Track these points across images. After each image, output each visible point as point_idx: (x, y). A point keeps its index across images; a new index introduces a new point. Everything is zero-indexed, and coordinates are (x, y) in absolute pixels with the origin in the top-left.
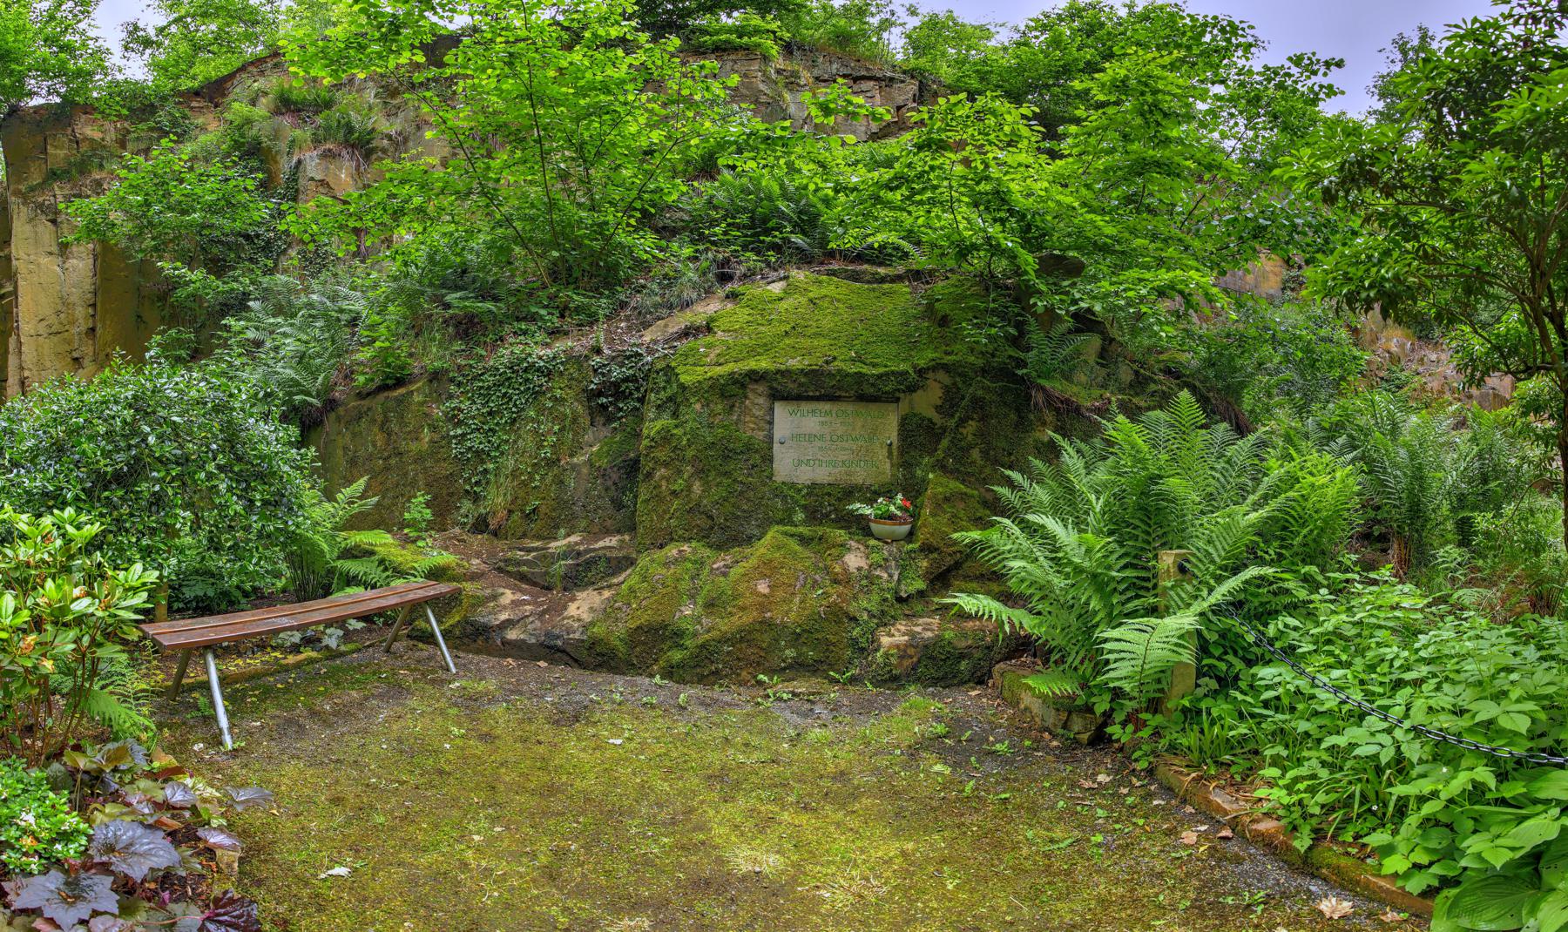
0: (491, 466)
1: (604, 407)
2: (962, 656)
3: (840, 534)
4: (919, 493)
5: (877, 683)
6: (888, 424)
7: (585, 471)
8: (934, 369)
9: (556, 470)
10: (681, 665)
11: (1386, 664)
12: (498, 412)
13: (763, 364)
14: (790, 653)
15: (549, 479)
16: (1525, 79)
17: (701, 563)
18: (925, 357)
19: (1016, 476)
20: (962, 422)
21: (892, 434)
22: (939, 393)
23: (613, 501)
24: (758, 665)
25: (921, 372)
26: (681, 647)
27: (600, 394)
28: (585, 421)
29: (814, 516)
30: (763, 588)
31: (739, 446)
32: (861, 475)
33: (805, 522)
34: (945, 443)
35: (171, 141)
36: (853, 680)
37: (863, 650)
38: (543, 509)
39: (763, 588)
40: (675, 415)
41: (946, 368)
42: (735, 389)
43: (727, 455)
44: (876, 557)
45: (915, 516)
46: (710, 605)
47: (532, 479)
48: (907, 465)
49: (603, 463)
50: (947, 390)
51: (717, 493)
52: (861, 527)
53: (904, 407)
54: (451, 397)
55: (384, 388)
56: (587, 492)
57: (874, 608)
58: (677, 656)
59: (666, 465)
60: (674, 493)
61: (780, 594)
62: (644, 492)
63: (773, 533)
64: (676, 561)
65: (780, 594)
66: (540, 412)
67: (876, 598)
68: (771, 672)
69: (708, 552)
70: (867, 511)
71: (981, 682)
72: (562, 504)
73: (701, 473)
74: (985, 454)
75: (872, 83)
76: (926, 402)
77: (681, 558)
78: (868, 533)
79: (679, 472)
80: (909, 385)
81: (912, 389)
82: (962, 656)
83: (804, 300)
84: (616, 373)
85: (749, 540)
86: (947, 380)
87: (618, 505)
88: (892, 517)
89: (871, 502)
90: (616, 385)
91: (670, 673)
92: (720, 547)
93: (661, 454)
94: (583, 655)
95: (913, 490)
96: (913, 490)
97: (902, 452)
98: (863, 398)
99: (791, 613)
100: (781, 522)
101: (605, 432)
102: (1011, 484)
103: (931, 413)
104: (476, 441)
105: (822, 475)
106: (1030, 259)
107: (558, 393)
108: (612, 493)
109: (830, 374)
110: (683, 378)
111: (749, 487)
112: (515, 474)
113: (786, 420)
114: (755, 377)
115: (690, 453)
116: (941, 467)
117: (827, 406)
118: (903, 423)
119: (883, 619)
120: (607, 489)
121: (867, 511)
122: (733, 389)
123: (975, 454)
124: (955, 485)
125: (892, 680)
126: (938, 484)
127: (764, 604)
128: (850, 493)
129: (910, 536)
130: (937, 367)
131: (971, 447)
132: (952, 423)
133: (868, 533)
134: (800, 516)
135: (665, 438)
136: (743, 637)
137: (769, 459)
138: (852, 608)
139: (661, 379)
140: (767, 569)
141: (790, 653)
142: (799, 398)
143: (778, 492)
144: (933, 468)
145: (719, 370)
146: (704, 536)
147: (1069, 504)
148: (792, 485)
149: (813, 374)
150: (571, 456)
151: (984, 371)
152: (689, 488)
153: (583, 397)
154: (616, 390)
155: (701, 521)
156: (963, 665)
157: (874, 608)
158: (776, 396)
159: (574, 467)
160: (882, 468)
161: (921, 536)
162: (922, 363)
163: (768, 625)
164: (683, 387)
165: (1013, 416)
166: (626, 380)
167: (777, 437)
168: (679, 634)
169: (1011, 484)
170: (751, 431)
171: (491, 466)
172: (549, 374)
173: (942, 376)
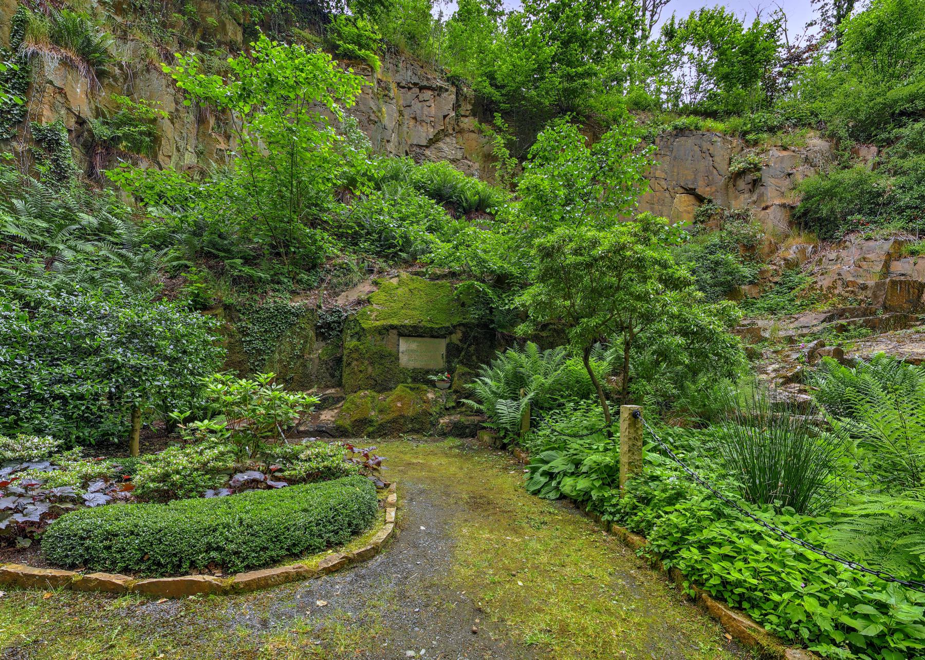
0: (266, 357)
1: (323, 333)
2: (467, 427)
3: (425, 387)
4: (453, 372)
5: (439, 435)
6: (441, 346)
7: (317, 361)
8: (459, 325)
9: (301, 360)
10: (373, 432)
11: (69, 243)
12: (270, 331)
13: (395, 322)
14: (410, 426)
15: (298, 364)
17: (373, 397)
18: (456, 320)
19: (484, 366)
20: (469, 345)
21: (443, 350)
22: (461, 335)
23: (330, 374)
24: (399, 431)
25: (454, 327)
26: (371, 426)
27: (321, 327)
28: (314, 339)
29: (415, 380)
30: (399, 405)
31: (386, 354)
32: (432, 365)
33: (412, 382)
34: (463, 353)
36: (431, 435)
37: (433, 425)
38: (296, 378)
39: (399, 405)
40: (359, 340)
41: (463, 325)
42: (384, 331)
43: (382, 357)
44: (438, 394)
45: (452, 380)
46: (381, 411)
47: (289, 364)
48: (449, 362)
49: (325, 358)
50: (464, 333)
51: (378, 371)
52: (432, 384)
53: (448, 340)
54: (240, 320)
56: (318, 370)
57: (438, 411)
58: (371, 429)
59: (357, 360)
60: (361, 371)
61: (405, 407)
62: (347, 371)
63: (400, 386)
64: (364, 397)
65: (405, 407)
66: (294, 333)
67: (438, 408)
68: (404, 433)
69: (375, 394)
70: (434, 378)
71: (473, 437)
72: (306, 376)
73: (372, 363)
74: (478, 358)
75: (430, 93)
76: (456, 338)
77: (365, 396)
78: (435, 386)
79: (362, 363)
80: (449, 332)
81: (451, 333)
82: (467, 427)
83: (407, 289)
84: (330, 319)
85: (391, 389)
86: (464, 330)
87: (333, 376)
88: (443, 380)
89: (436, 375)
90: (329, 324)
91: (369, 435)
92: (379, 392)
93: (355, 356)
94: (334, 432)
95: (451, 371)
96: (451, 371)
97: (447, 358)
98: (432, 337)
99: (410, 413)
100: (402, 382)
101: (323, 344)
102: (482, 369)
103: (458, 342)
104: (258, 344)
105: (418, 364)
107: (303, 326)
108: (330, 371)
109: (421, 328)
110: (364, 326)
111: (391, 369)
112: (280, 361)
114: (392, 327)
115: (367, 356)
116: (461, 362)
117: (419, 339)
118: (448, 345)
119: (441, 415)
120: (327, 369)
121: (434, 378)
122: (384, 331)
123: (474, 358)
124: (467, 369)
125: (444, 435)
126: (460, 369)
127: (400, 409)
128: (428, 372)
129: (450, 388)
130: (460, 325)
131: (473, 355)
132: (465, 346)
133: (435, 386)
134: (410, 380)
135: (357, 349)
136: (394, 421)
137: (398, 359)
138: (431, 411)
139: (352, 324)
140: (400, 398)
141: (410, 426)
142: (409, 336)
143: (401, 372)
144: (458, 363)
145: (378, 323)
146: (373, 388)
148: (407, 369)
149: (415, 327)
150: (310, 354)
151: (478, 326)
152: (367, 369)
153: (314, 328)
154: (328, 326)
155: (372, 382)
156: (467, 430)
157: (438, 411)
158: (401, 335)
159: (311, 360)
160: (441, 363)
161: (454, 387)
162: (455, 323)
163: (403, 416)
164: (363, 329)
165: (489, 343)
166: (334, 322)
167: (401, 350)
168: (371, 421)
169: (482, 369)
170: (390, 348)
171: (266, 357)
172: (297, 316)
173: (461, 328)
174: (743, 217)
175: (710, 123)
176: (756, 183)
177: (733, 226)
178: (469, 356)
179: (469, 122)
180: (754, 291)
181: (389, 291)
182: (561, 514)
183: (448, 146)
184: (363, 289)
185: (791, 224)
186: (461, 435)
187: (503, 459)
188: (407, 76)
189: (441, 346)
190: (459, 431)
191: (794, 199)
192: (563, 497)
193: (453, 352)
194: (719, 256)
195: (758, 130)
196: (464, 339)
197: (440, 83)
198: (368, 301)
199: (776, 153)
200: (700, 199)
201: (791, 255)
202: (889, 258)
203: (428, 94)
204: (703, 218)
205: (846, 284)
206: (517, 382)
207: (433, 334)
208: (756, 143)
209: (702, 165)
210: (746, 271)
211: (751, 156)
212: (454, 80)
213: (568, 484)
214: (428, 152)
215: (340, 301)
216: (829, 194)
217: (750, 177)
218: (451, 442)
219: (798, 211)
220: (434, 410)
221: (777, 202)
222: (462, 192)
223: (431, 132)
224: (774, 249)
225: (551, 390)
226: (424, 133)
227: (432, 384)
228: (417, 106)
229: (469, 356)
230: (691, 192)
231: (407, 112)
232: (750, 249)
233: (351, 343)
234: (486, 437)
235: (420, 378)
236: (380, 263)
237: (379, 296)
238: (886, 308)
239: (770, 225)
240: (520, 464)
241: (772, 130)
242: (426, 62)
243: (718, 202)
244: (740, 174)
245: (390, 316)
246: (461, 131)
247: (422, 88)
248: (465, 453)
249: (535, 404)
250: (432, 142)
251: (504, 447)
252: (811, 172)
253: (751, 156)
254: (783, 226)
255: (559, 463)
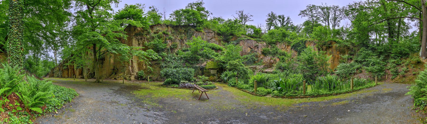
6: (216, 70)
13: (210, 68)
16: (331, 8)
18: (218, 67)
29: (213, 75)
32: (215, 73)
35: (377, 102)
52: (215, 76)
55: (106, 96)
76: (218, 70)
80: (217, 69)
99: (213, 79)
105: (213, 73)
106: (166, 54)
113: (211, 71)
119: (217, 79)
122: (209, 69)
125: (217, 82)
126: (219, 74)
135: (205, 71)
147: (224, 75)
154: (201, 68)
158: (211, 69)
160: (216, 73)
170: (210, 71)
174: (256, 52)
175: (252, 39)
176: (258, 48)
177: (255, 53)
178: (220, 72)
179: (216, 36)
180: (257, 62)
181: (208, 63)
182: (231, 87)
183: (213, 40)
184: (205, 63)
185: (262, 53)
186: (219, 82)
187: (225, 84)
188: (207, 31)
189: (216, 70)
190: (219, 81)
191: (262, 50)
192: (232, 86)
193: (217, 71)
194: (253, 57)
195: (258, 41)
196: (219, 70)
197: (212, 32)
198: (206, 65)
199: (260, 44)
200: (251, 48)
201: (262, 57)
202: (270, 59)
203: (210, 33)
204: (251, 51)
205: (266, 62)
206: (226, 75)
207: (215, 69)
208: (258, 42)
209: (251, 44)
210: (256, 59)
211: (257, 44)
212: (214, 31)
213: (232, 85)
214: (210, 41)
215: (202, 65)
216: (265, 50)
217: (257, 47)
218: (218, 83)
219: (262, 52)
220: (216, 79)
221: (260, 50)
222: (216, 48)
223: (211, 38)
224: (260, 57)
225: (230, 76)
226: (209, 38)
227: (215, 76)
228: (208, 35)
229: (220, 72)
230: (250, 47)
231: (207, 36)
232: (257, 56)
233: (205, 71)
234: (223, 82)
235: (214, 75)
236: (207, 60)
237: (207, 64)
238: (269, 65)
239: (259, 53)
240: (227, 84)
241: (260, 41)
242: (209, 29)
243: (253, 49)
244: (256, 46)
245: (209, 67)
246: (215, 37)
247: (209, 33)
248: (221, 84)
249: (229, 78)
250: (210, 39)
251: (225, 83)
252: (264, 47)
253: (257, 44)
254: (261, 54)
255: (231, 83)
